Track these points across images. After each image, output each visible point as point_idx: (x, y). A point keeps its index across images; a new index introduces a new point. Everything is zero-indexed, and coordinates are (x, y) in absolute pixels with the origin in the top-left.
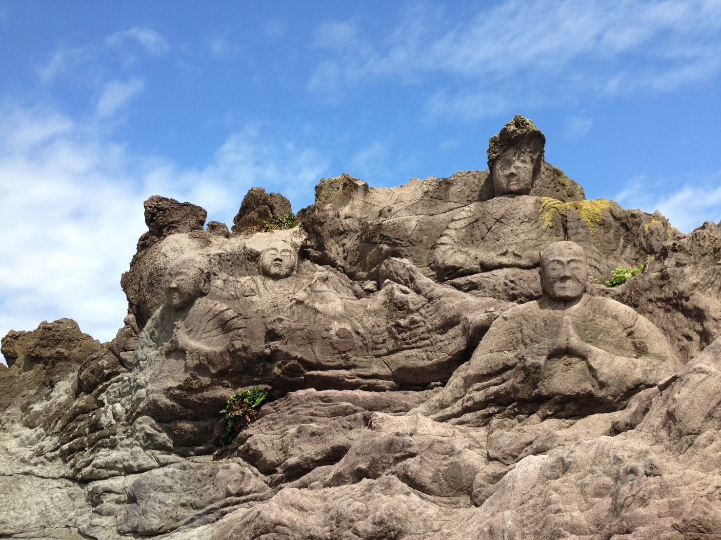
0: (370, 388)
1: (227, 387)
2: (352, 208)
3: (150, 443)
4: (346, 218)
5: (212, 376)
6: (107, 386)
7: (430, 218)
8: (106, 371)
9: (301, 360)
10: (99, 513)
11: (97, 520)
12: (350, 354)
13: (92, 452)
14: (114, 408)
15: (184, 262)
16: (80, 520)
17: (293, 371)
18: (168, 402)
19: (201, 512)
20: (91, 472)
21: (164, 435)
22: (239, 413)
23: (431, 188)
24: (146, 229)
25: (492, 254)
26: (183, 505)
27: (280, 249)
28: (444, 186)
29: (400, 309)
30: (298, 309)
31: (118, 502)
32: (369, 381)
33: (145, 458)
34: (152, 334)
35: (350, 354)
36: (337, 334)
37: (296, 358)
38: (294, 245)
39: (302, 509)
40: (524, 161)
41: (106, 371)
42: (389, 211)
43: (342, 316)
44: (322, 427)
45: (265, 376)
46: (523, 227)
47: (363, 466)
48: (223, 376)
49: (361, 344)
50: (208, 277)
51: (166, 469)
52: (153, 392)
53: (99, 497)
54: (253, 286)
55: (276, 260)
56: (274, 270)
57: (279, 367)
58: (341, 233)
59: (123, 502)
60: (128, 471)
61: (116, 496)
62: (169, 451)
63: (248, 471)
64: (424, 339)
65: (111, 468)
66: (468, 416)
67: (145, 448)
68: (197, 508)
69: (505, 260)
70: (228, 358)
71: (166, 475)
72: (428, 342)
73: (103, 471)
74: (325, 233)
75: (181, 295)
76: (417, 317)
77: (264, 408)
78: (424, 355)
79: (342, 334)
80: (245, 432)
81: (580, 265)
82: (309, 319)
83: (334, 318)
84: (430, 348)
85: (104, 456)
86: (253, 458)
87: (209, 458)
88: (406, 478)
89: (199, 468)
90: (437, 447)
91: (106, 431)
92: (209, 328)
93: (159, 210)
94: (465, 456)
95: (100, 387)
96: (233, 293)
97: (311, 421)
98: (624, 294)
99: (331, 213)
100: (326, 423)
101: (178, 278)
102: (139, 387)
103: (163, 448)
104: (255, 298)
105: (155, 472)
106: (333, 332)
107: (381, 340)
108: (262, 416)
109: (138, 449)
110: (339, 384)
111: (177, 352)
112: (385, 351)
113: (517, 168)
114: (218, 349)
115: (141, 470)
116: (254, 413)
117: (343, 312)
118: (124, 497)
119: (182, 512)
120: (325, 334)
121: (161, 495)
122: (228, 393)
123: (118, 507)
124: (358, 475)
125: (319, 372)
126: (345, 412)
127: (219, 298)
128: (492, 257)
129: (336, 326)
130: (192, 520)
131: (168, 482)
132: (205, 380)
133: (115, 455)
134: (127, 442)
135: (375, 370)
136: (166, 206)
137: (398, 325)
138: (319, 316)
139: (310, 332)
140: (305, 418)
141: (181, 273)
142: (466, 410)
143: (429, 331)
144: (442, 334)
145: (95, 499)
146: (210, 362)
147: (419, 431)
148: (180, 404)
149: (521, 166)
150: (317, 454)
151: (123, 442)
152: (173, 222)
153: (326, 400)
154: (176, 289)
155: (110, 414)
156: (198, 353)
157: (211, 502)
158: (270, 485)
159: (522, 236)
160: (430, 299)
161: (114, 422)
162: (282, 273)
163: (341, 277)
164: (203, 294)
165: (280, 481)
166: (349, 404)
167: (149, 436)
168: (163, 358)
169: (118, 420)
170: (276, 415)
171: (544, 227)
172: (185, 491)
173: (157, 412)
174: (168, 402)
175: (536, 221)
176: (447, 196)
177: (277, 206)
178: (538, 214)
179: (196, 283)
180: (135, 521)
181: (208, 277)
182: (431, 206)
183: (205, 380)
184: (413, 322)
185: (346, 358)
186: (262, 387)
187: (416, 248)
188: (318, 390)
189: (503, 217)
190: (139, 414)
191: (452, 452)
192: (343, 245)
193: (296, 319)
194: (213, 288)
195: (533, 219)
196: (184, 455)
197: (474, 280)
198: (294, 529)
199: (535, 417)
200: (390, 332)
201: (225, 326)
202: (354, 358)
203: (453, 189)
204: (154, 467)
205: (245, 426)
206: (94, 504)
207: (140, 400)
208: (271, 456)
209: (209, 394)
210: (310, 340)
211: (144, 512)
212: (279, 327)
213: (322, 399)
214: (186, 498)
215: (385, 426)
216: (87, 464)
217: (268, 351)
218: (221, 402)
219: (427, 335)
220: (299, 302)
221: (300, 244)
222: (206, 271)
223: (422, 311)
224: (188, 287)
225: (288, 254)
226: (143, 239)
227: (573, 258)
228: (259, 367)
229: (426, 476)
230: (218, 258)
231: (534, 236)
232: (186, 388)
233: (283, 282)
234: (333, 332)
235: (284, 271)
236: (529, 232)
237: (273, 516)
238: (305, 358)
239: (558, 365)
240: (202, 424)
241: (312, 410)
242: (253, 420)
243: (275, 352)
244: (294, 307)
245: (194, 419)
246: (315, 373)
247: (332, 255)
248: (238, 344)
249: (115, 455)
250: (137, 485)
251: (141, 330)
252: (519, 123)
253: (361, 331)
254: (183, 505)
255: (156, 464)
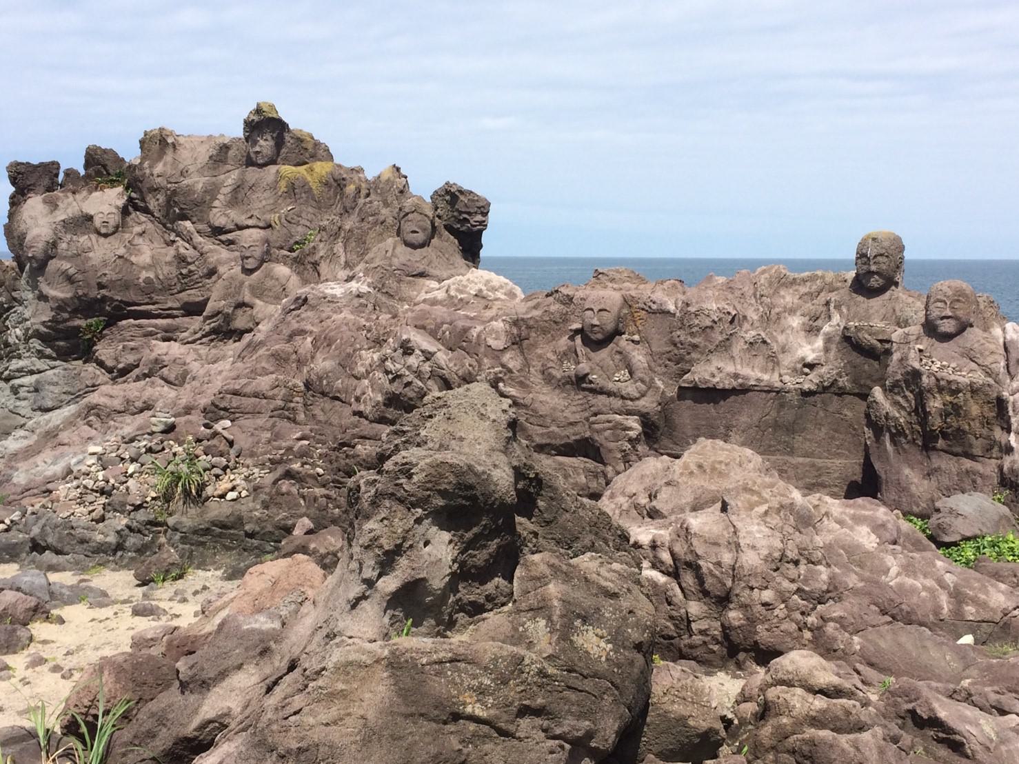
0: (168, 316)
1: (81, 319)
2: (165, 165)
3: (41, 355)
4: (158, 176)
5: (69, 313)
6: (8, 316)
7: (214, 178)
8: (5, 306)
9: (121, 301)
10: (18, 399)
11: (18, 403)
12: (153, 295)
13: (8, 361)
14: (15, 332)
15: (34, 238)
16: (8, 403)
17: (117, 308)
18: (45, 330)
19: (73, 397)
20: (9, 374)
21: (49, 349)
22: (89, 336)
23: (215, 152)
24: (13, 189)
25: (243, 217)
26: (64, 393)
27: (106, 213)
28: (224, 150)
29: (183, 261)
30: (119, 262)
31: (29, 392)
32: (167, 312)
33: (40, 364)
34: (28, 282)
35: (153, 295)
36: (144, 282)
37: (117, 300)
38: (117, 207)
39: (111, 397)
40: (266, 140)
41: (5, 306)
42: (187, 172)
43: (150, 266)
44: (140, 343)
45: (102, 312)
46: (265, 194)
47: (146, 371)
48: (75, 313)
49: (160, 287)
50: (54, 245)
51: (54, 371)
52: (35, 324)
53: (16, 390)
54: (89, 245)
55: (104, 222)
56: (103, 231)
57: (109, 306)
58: (156, 190)
59: (32, 392)
60: (32, 373)
61: (27, 389)
62: (55, 359)
63: (98, 372)
64: (198, 283)
65: (21, 372)
66: (204, 340)
67: (39, 358)
68: (72, 394)
69: (250, 222)
70: (76, 301)
71: (55, 374)
72: (200, 284)
73: (17, 373)
74: (144, 190)
75: (37, 261)
76: (192, 267)
77: (104, 332)
78: (199, 293)
79: (148, 281)
80: (95, 348)
81: (256, 248)
82: (127, 270)
83: (144, 268)
84: (202, 289)
85: (15, 364)
86: (101, 364)
87: (80, 362)
88: (162, 378)
89: (75, 369)
90: (178, 361)
91: (14, 348)
92: (60, 281)
93: (19, 173)
94: (190, 366)
95: (4, 316)
96: (75, 252)
97: (132, 340)
98: (298, 257)
99: (148, 171)
100: (140, 341)
101: (32, 250)
102: (27, 320)
103: (49, 357)
104: (91, 255)
105: (48, 373)
106: (141, 280)
107: (173, 283)
108: (104, 337)
109: (34, 359)
110: (148, 315)
111: (42, 297)
112: (176, 291)
113: (261, 146)
114: (69, 295)
115: (40, 372)
116: (99, 336)
117: (151, 263)
118: (32, 389)
119: (64, 397)
120: (136, 282)
121: (52, 388)
122: (81, 323)
123: (29, 395)
124: (146, 376)
125: (136, 308)
126: (151, 334)
127: (65, 258)
128: (242, 219)
129: (144, 275)
130: (69, 401)
131: (55, 379)
132: (66, 315)
133: (21, 363)
134: (27, 354)
135: (170, 304)
136: (23, 171)
137: (181, 274)
138: (134, 267)
139: (126, 281)
140: (129, 338)
141: (33, 247)
142: (204, 336)
143: (201, 277)
144: (209, 279)
145: (15, 390)
146: (66, 304)
147: (170, 353)
148: (54, 331)
149: (265, 144)
150: (135, 361)
151: (25, 355)
152: (30, 186)
153: (140, 326)
154: (33, 257)
155: (14, 337)
156: (55, 299)
157: (79, 391)
158: (112, 380)
159: (264, 203)
160: (202, 254)
161: (17, 341)
162: (109, 232)
163: (157, 227)
164: (52, 258)
165: (116, 377)
166: (153, 329)
167: (39, 351)
168: (37, 301)
169: (20, 340)
170: (112, 337)
171: (280, 193)
172: (66, 384)
173: (38, 335)
174: (45, 330)
175: (275, 189)
176: (226, 158)
177: (109, 163)
178: (277, 182)
179: (46, 251)
180: (39, 404)
181: (54, 245)
182: (215, 169)
183: (66, 315)
184: (190, 271)
185: (151, 298)
186: (102, 318)
187: (200, 208)
188: (135, 319)
189: (253, 185)
190: (30, 338)
191: (184, 364)
192: (158, 200)
193: (117, 271)
194: (59, 251)
195: (274, 186)
196: (66, 361)
197: (231, 238)
198: (106, 407)
199: (231, 341)
200: (178, 279)
201: (70, 279)
202: (157, 297)
203: (231, 153)
204: (47, 370)
205: (95, 344)
206: (15, 394)
207: (28, 329)
208: (110, 363)
209: (70, 324)
210: (126, 286)
211: (43, 398)
212: (104, 280)
213: (137, 326)
214: (66, 389)
215: (155, 349)
216: (6, 369)
217: (99, 296)
218: (78, 328)
219: (200, 280)
220: (120, 257)
221: (121, 206)
222: (51, 241)
223: (196, 263)
224: (40, 255)
225: (113, 216)
226: (12, 197)
227: (252, 244)
228: (97, 306)
229: (172, 377)
230: (62, 223)
231: (272, 201)
232: (54, 320)
233: (111, 239)
234: (141, 280)
235: (111, 230)
236: (269, 198)
237: (95, 402)
238: (124, 299)
239: (240, 312)
240: (72, 341)
241: (131, 333)
242: (99, 340)
243: (104, 297)
244: (117, 261)
245: (65, 339)
246: (133, 308)
247: (151, 208)
248: (80, 292)
249: (21, 363)
250: (38, 382)
251: (22, 273)
252: (258, 111)
253: (161, 277)
254: (64, 393)
255: (48, 368)
